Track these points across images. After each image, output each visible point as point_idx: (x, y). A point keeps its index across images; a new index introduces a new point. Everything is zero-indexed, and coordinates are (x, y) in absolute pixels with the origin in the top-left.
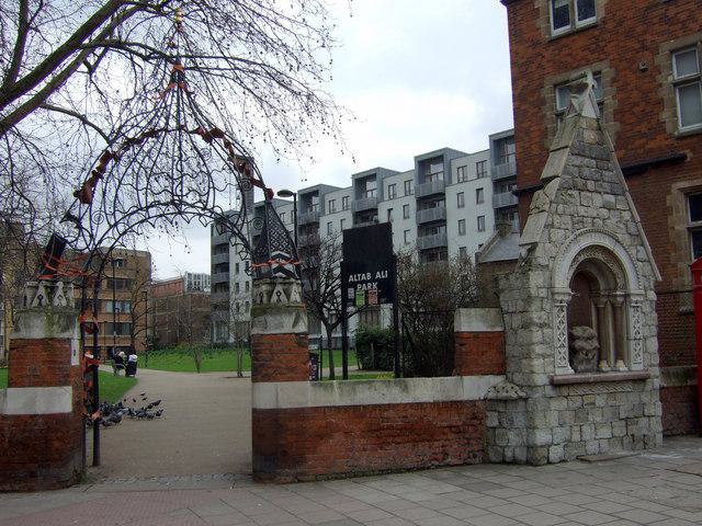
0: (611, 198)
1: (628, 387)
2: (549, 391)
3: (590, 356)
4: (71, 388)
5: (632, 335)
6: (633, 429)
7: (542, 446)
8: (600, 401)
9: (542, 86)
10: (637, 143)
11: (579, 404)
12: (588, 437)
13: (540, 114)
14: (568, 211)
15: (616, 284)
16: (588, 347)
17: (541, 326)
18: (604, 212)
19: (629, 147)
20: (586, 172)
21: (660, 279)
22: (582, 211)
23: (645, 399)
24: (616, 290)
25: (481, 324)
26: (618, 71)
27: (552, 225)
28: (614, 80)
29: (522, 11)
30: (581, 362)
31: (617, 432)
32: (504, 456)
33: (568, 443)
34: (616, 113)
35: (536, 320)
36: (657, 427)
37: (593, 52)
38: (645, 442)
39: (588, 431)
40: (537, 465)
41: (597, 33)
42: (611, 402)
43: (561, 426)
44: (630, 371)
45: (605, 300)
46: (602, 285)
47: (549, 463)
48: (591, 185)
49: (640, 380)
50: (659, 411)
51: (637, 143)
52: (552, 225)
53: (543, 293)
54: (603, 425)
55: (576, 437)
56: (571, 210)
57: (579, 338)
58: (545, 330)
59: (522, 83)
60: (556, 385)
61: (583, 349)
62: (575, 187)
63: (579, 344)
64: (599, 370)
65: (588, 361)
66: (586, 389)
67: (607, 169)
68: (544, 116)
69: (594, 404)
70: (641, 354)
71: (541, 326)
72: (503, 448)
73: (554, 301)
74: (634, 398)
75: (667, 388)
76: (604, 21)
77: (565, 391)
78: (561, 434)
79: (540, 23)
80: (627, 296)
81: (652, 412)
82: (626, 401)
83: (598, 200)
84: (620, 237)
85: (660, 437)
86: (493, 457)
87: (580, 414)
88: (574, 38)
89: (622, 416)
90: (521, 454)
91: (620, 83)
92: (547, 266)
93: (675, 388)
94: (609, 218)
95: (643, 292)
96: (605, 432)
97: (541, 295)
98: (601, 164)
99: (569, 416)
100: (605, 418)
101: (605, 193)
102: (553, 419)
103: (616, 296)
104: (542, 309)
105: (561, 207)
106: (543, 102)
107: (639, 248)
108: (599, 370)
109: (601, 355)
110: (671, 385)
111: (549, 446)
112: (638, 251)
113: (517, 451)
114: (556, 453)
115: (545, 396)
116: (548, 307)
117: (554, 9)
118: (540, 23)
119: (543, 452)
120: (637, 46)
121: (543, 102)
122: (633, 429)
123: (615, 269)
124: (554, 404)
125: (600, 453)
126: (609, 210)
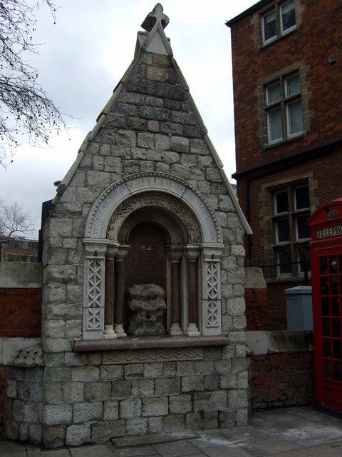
0: (185, 141)
1: (198, 355)
2: (70, 359)
3: (153, 318)
4: (312, 329)
5: (206, 294)
6: (202, 405)
7: (55, 426)
8: (151, 371)
9: (255, 87)
10: (327, 126)
11: (118, 373)
12: (130, 415)
13: (253, 110)
14: (116, 152)
15: (189, 236)
16: (150, 308)
17: (65, 282)
18: (173, 156)
19: (321, 130)
20: (147, 111)
21: (250, 232)
22: (138, 153)
23: (222, 368)
24: (187, 244)
25: (9, 279)
26: (312, 67)
27: (91, 167)
28: (309, 75)
29: (241, 30)
30: (140, 325)
31: (177, 408)
32: (19, 434)
33: (96, 422)
34: (310, 102)
35: (56, 275)
36: (240, 401)
37: (293, 54)
38: (220, 421)
39: (129, 408)
40: (50, 449)
41: (296, 37)
42: (167, 373)
43: (87, 400)
44: (202, 335)
45: (178, 254)
46: (174, 238)
47: (66, 446)
48: (153, 125)
49: (216, 348)
50: (244, 383)
51: (327, 126)
52: (91, 167)
53: (70, 243)
54: (156, 399)
55: (111, 414)
56: (122, 151)
57: (135, 297)
58: (70, 287)
59: (241, 86)
60: (85, 353)
61: (140, 310)
62: (129, 127)
63: (135, 304)
64: (167, 334)
65: (151, 324)
66: (131, 358)
67: (180, 109)
68: (256, 111)
69: (142, 375)
70: (218, 316)
71: (65, 282)
72: (19, 423)
73: (85, 253)
74: (205, 368)
75: (280, 354)
76: (301, 27)
77: (96, 360)
78: (86, 411)
79: (254, 37)
80: (200, 250)
81: (233, 383)
82: (191, 374)
83: (163, 142)
84: (192, 184)
85: (243, 415)
86: (10, 434)
87: (119, 389)
88: (280, 43)
89: (185, 389)
90: (36, 433)
91: (314, 77)
92: (80, 213)
93: (289, 354)
94: (179, 162)
95: (221, 245)
96: (161, 409)
97: (68, 246)
98: (170, 103)
99: (99, 390)
100: (159, 391)
101: (174, 135)
102: (75, 393)
103: (187, 249)
104: (67, 262)
105: (106, 148)
106: (255, 100)
107: (222, 197)
108: (167, 334)
109: (165, 320)
110: (284, 350)
111: (67, 425)
112: (220, 200)
113: (33, 428)
114: (75, 434)
115: (64, 365)
116: (76, 260)
117: (265, 24)
118: (254, 37)
119: (59, 433)
120: (327, 43)
121: (255, 100)
122: (202, 405)
123: (186, 219)
124: (78, 375)
125: (148, 433)
126: (180, 153)
